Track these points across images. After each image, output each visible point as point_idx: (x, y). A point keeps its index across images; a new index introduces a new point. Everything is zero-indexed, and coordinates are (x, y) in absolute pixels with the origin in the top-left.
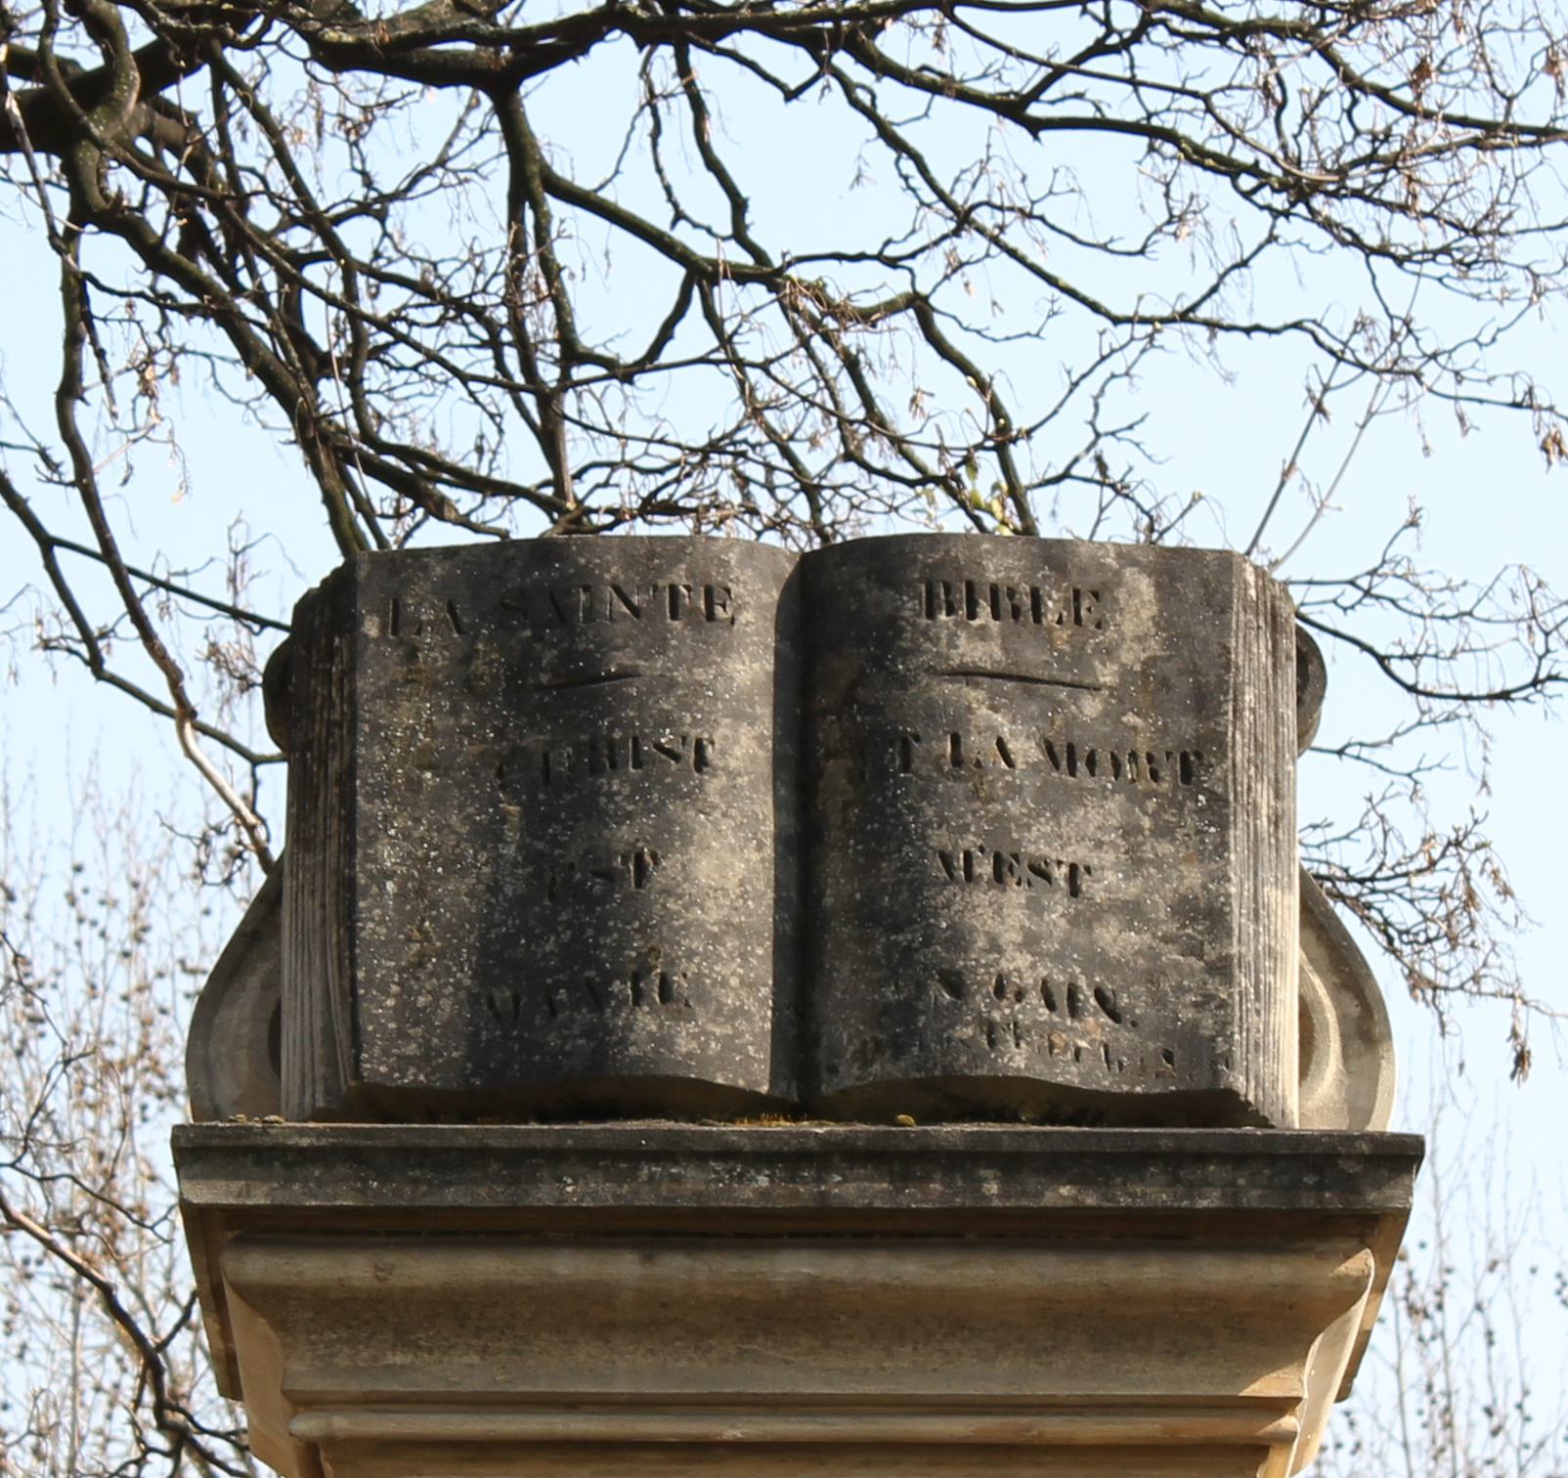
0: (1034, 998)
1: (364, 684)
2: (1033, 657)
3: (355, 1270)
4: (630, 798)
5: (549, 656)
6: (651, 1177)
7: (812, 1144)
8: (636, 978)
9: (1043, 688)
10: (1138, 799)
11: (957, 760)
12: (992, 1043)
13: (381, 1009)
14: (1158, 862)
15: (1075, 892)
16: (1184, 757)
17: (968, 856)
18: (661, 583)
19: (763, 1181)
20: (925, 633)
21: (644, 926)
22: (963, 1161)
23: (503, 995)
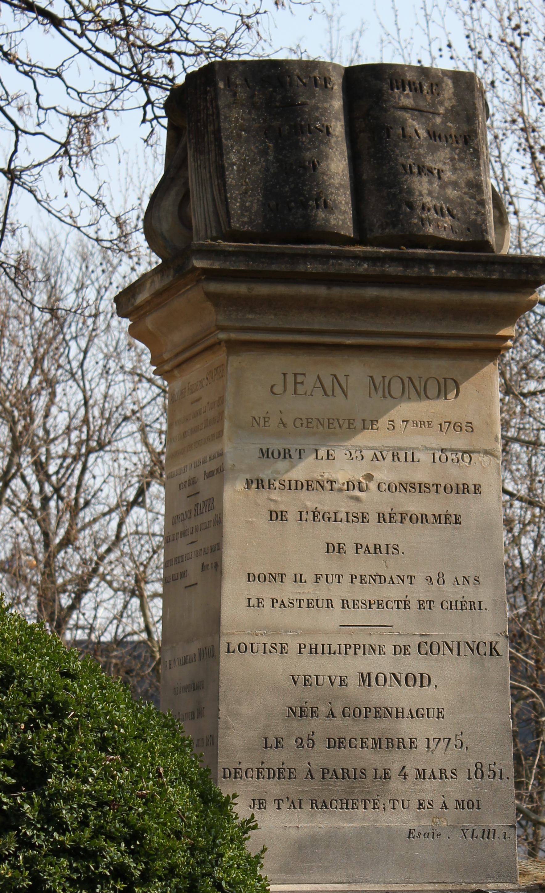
0: (433, 211)
1: (221, 103)
2: (422, 104)
3: (242, 289)
4: (309, 143)
5: (278, 97)
6: (333, 264)
7: (381, 255)
8: (317, 200)
9: (425, 114)
10: (453, 149)
11: (404, 136)
12: (423, 224)
13: (235, 206)
14: (461, 169)
15: (440, 178)
16: (465, 137)
17: (410, 166)
18: (312, 76)
19: (366, 266)
20: (391, 95)
21: (317, 184)
22: (424, 261)
23: (273, 203)
